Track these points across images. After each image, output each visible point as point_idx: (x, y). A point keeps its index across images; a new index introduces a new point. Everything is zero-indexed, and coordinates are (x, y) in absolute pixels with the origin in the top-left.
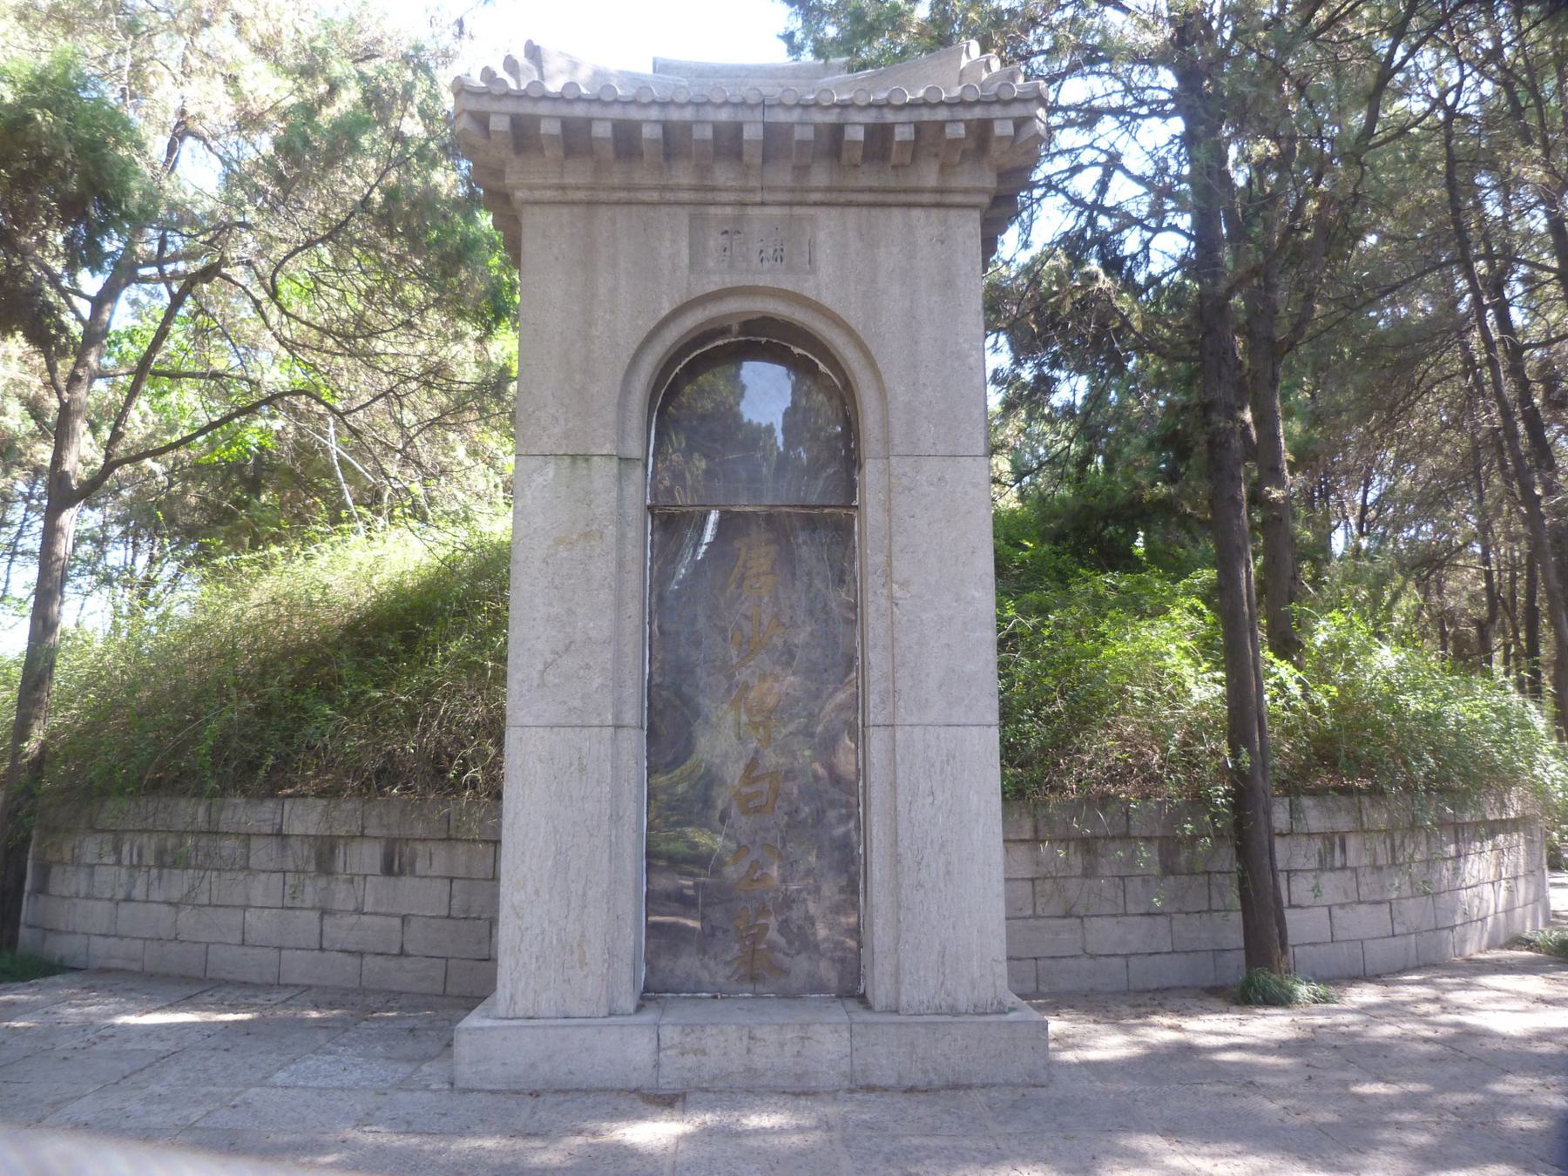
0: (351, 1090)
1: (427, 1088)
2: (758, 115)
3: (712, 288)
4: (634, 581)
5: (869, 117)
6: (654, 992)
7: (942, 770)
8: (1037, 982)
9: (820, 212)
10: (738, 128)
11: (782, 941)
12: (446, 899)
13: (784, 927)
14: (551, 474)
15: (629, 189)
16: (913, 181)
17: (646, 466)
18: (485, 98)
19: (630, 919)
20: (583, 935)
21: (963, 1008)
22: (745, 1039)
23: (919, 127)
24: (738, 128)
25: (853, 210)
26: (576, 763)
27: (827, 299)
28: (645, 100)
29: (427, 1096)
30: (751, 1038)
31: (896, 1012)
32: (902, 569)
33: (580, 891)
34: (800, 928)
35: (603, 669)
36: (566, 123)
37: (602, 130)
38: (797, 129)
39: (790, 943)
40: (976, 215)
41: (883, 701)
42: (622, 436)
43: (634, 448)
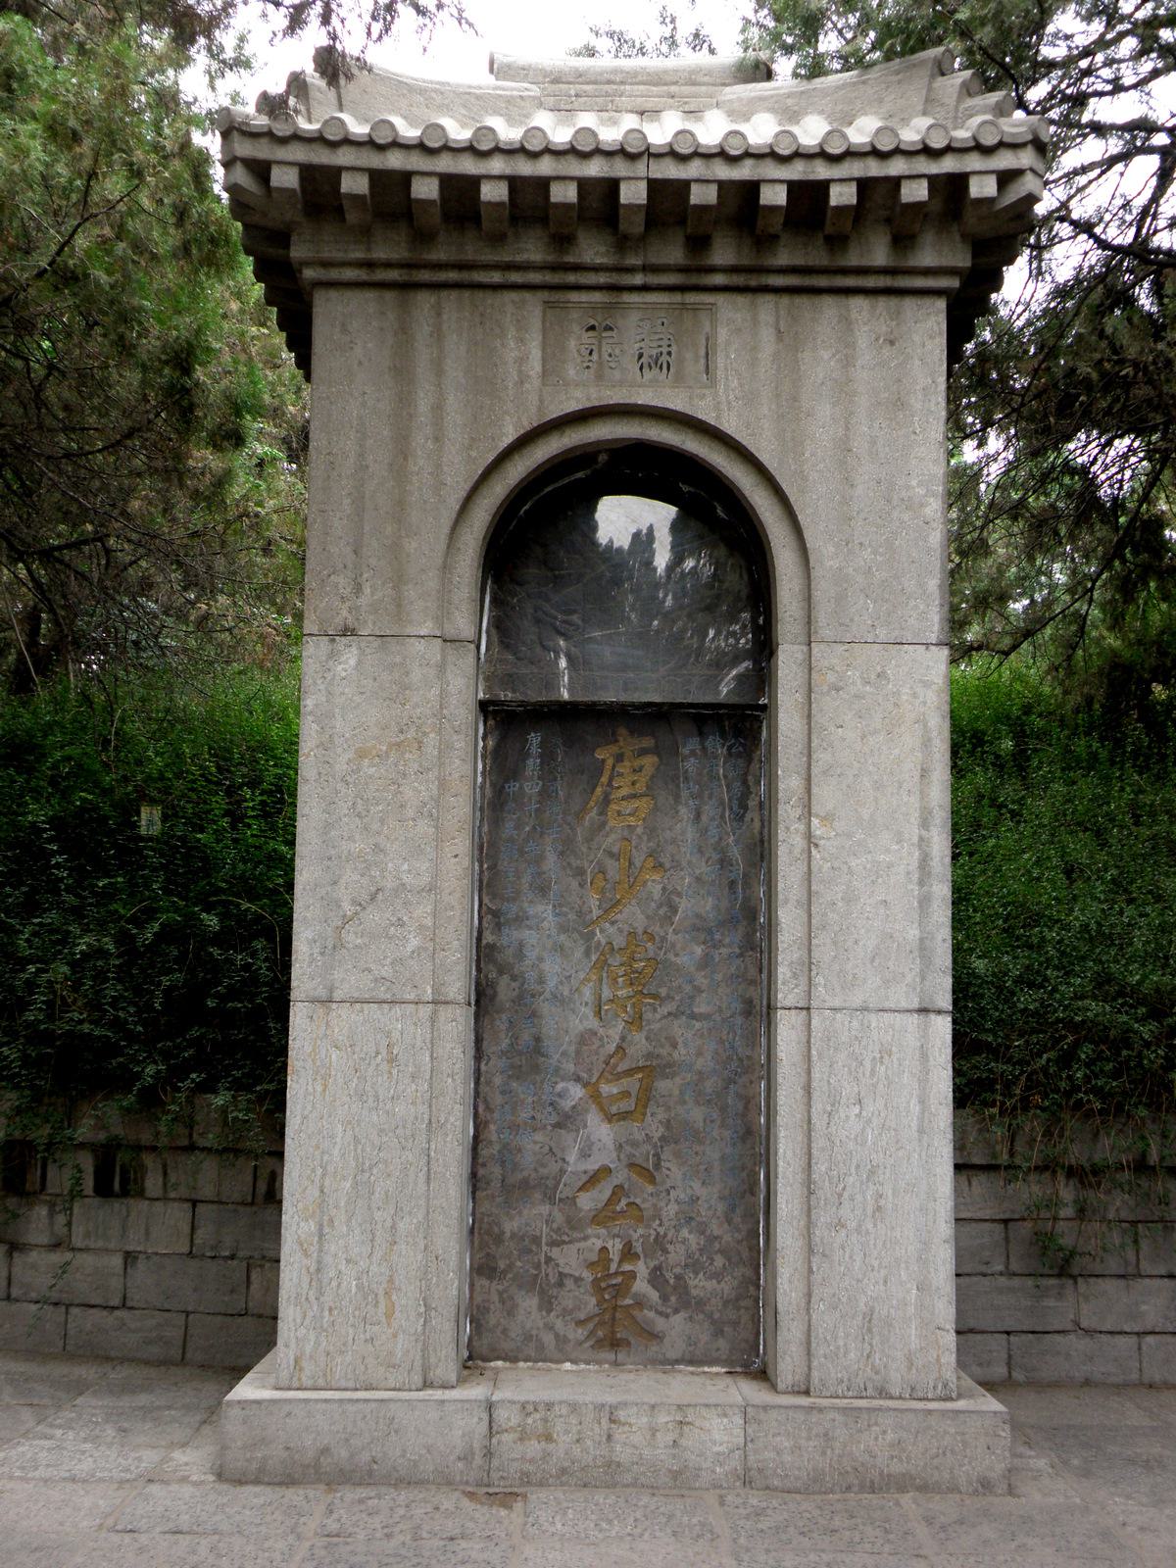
0: (84, 1481)
1: (184, 1479)
2: (640, 168)
3: (572, 406)
4: (461, 809)
5: (797, 171)
6: (476, 1357)
7: (873, 1072)
8: (1009, 1365)
9: (720, 299)
10: (612, 185)
11: (654, 1295)
12: (187, 1229)
13: (656, 1277)
14: (352, 662)
15: (461, 266)
16: (853, 259)
17: (478, 647)
18: (264, 141)
19: (453, 1262)
20: (391, 1280)
21: (896, 1391)
22: (604, 1422)
23: (864, 185)
24: (612, 185)
25: (769, 298)
26: (384, 1052)
27: (730, 425)
28: (484, 147)
29: (187, 1491)
30: (612, 1421)
31: (807, 1393)
32: (826, 795)
33: (389, 1223)
34: (678, 1277)
35: (421, 927)
36: (377, 177)
37: (425, 190)
38: (694, 188)
39: (665, 1298)
40: (941, 304)
41: (795, 976)
42: (443, 613)
43: (463, 623)
